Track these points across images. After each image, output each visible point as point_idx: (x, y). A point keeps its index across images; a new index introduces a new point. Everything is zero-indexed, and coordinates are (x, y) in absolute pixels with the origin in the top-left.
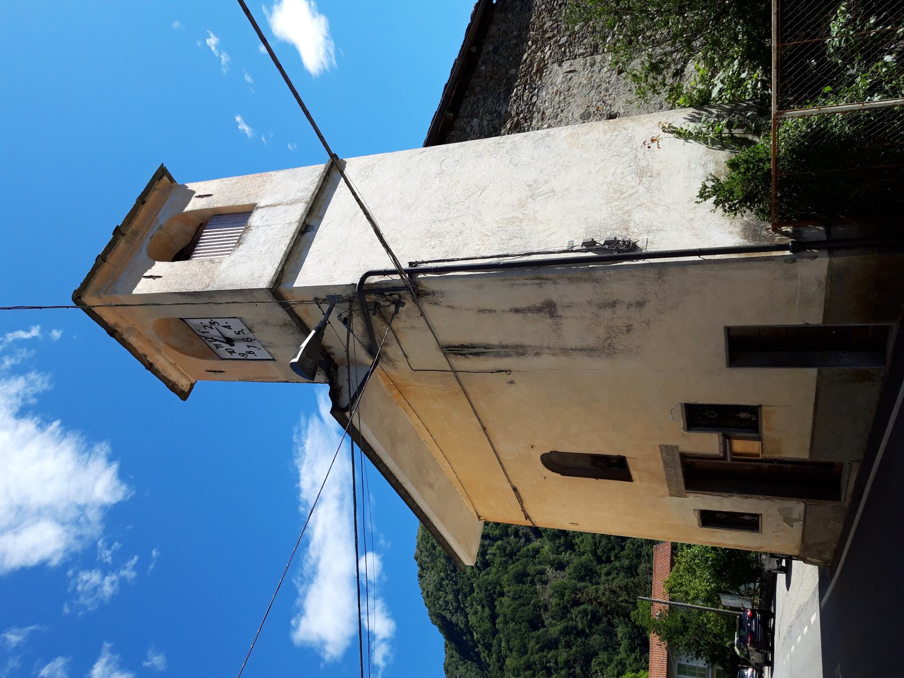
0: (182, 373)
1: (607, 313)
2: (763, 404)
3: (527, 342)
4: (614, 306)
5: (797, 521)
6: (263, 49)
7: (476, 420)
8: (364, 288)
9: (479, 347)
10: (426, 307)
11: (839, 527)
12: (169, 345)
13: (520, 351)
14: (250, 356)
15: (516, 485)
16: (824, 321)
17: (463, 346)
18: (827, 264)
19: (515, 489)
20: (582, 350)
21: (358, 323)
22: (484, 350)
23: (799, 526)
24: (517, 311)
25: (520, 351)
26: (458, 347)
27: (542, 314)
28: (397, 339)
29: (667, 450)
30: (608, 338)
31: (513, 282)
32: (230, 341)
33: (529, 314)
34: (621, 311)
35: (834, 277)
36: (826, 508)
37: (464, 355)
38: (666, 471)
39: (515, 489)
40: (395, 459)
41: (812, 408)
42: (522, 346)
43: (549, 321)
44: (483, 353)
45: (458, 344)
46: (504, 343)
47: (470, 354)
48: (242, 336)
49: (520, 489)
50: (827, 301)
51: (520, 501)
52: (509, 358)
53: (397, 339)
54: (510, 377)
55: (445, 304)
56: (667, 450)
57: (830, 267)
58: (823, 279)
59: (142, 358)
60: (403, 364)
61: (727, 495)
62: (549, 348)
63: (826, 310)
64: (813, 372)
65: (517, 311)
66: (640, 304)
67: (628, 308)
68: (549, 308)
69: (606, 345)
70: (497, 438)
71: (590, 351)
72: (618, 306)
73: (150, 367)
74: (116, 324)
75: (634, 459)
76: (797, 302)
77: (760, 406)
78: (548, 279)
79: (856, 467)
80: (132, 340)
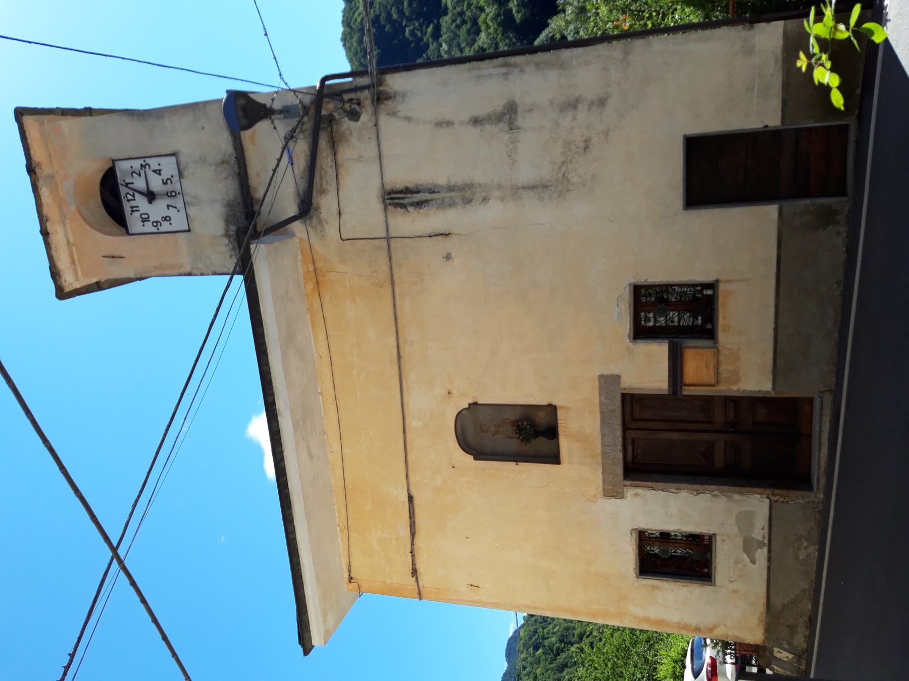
0: (73, 262)
1: (567, 120)
2: (721, 278)
3: (478, 177)
4: (575, 107)
5: (760, 545)
6: (259, 428)
7: (392, 341)
8: (325, 91)
11: (813, 549)
12: (80, 213)
14: (165, 227)
15: (414, 492)
16: (783, 122)
17: (407, 191)
19: (411, 498)
21: (301, 147)
22: (427, 196)
23: (762, 554)
26: (401, 192)
27: (501, 125)
28: (338, 183)
29: (608, 382)
32: (151, 196)
33: (488, 127)
36: (798, 499)
37: (404, 206)
38: (603, 435)
39: (411, 498)
40: (285, 356)
41: (773, 282)
42: (469, 186)
44: (427, 201)
48: (169, 188)
49: (416, 501)
51: (413, 534)
52: (454, 210)
53: (338, 183)
56: (608, 382)
57: (785, 34)
58: (779, 51)
59: (43, 219)
60: (332, 231)
62: (500, 187)
63: (784, 102)
64: (771, 211)
68: (508, 116)
69: (560, 175)
71: (539, 188)
72: (580, 107)
73: (45, 233)
74: (39, 164)
75: (567, 409)
76: (756, 90)
79: (828, 399)
80: (45, 192)
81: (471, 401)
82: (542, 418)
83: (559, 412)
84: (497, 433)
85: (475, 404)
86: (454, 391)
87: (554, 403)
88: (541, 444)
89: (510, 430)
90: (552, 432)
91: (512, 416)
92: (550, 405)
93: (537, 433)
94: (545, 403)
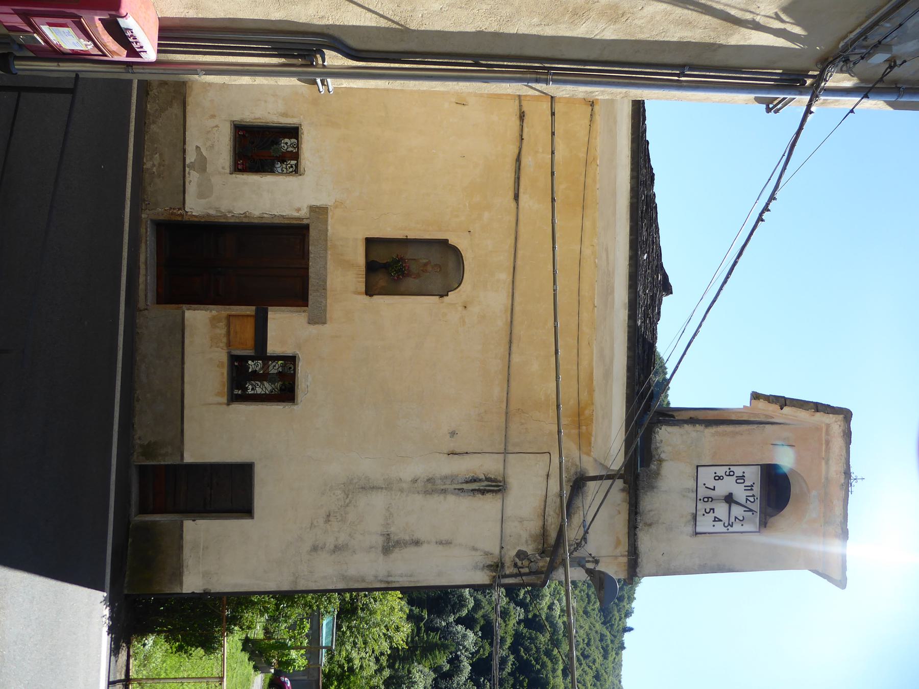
1: (343, 538)
3: (419, 499)
4: (335, 547)
9: (468, 491)
10: (496, 551)
13: (432, 487)
17: (483, 492)
18: (184, 587)
19: (516, 197)
20: (373, 488)
22: (465, 486)
23: (191, 158)
24: (417, 543)
25: (432, 487)
26: (489, 491)
27: (396, 538)
29: (318, 319)
30: (347, 505)
31: (410, 579)
32: (729, 499)
33: (407, 538)
34: (330, 542)
35: (177, 575)
36: (161, 212)
37: (488, 479)
38: (325, 268)
43: (393, 529)
44: (467, 482)
45: (489, 496)
46: (442, 497)
47: (480, 480)
49: (511, 194)
50: (181, 548)
51: (518, 160)
52: (443, 474)
53: (546, 501)
54: (452, 445)
55: (478, 553)
56: (318, 319)
57: (181, 584)
58: (186, 573)
61: (276, 221)
64: (188, 458)
65: (417, 543)
66: (315, 549)
67: (325, 544)
69: (350, 496)
70: (501, 323)
71: (368, 487)
72: (332, 547)
77: (228, 404)
78: (381, 581)
81: (445, 298)
82: (381, 280)
83: (364, 289)
84: (426, 265)
85: (441, 296)
86: (460, 309)
87: (368, 297)
88: (383, 256)
89: (414, 268)
90: (372, 267)
91: (411, 283)
92: (371, 296)
93: (386, 267)
94: (375, 297)
